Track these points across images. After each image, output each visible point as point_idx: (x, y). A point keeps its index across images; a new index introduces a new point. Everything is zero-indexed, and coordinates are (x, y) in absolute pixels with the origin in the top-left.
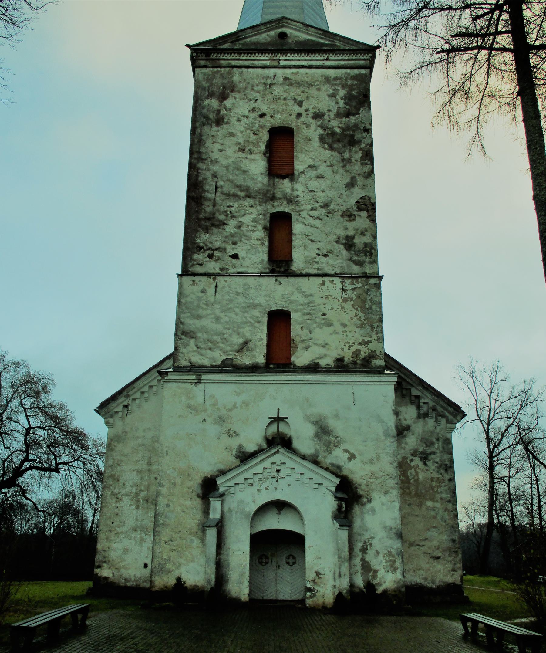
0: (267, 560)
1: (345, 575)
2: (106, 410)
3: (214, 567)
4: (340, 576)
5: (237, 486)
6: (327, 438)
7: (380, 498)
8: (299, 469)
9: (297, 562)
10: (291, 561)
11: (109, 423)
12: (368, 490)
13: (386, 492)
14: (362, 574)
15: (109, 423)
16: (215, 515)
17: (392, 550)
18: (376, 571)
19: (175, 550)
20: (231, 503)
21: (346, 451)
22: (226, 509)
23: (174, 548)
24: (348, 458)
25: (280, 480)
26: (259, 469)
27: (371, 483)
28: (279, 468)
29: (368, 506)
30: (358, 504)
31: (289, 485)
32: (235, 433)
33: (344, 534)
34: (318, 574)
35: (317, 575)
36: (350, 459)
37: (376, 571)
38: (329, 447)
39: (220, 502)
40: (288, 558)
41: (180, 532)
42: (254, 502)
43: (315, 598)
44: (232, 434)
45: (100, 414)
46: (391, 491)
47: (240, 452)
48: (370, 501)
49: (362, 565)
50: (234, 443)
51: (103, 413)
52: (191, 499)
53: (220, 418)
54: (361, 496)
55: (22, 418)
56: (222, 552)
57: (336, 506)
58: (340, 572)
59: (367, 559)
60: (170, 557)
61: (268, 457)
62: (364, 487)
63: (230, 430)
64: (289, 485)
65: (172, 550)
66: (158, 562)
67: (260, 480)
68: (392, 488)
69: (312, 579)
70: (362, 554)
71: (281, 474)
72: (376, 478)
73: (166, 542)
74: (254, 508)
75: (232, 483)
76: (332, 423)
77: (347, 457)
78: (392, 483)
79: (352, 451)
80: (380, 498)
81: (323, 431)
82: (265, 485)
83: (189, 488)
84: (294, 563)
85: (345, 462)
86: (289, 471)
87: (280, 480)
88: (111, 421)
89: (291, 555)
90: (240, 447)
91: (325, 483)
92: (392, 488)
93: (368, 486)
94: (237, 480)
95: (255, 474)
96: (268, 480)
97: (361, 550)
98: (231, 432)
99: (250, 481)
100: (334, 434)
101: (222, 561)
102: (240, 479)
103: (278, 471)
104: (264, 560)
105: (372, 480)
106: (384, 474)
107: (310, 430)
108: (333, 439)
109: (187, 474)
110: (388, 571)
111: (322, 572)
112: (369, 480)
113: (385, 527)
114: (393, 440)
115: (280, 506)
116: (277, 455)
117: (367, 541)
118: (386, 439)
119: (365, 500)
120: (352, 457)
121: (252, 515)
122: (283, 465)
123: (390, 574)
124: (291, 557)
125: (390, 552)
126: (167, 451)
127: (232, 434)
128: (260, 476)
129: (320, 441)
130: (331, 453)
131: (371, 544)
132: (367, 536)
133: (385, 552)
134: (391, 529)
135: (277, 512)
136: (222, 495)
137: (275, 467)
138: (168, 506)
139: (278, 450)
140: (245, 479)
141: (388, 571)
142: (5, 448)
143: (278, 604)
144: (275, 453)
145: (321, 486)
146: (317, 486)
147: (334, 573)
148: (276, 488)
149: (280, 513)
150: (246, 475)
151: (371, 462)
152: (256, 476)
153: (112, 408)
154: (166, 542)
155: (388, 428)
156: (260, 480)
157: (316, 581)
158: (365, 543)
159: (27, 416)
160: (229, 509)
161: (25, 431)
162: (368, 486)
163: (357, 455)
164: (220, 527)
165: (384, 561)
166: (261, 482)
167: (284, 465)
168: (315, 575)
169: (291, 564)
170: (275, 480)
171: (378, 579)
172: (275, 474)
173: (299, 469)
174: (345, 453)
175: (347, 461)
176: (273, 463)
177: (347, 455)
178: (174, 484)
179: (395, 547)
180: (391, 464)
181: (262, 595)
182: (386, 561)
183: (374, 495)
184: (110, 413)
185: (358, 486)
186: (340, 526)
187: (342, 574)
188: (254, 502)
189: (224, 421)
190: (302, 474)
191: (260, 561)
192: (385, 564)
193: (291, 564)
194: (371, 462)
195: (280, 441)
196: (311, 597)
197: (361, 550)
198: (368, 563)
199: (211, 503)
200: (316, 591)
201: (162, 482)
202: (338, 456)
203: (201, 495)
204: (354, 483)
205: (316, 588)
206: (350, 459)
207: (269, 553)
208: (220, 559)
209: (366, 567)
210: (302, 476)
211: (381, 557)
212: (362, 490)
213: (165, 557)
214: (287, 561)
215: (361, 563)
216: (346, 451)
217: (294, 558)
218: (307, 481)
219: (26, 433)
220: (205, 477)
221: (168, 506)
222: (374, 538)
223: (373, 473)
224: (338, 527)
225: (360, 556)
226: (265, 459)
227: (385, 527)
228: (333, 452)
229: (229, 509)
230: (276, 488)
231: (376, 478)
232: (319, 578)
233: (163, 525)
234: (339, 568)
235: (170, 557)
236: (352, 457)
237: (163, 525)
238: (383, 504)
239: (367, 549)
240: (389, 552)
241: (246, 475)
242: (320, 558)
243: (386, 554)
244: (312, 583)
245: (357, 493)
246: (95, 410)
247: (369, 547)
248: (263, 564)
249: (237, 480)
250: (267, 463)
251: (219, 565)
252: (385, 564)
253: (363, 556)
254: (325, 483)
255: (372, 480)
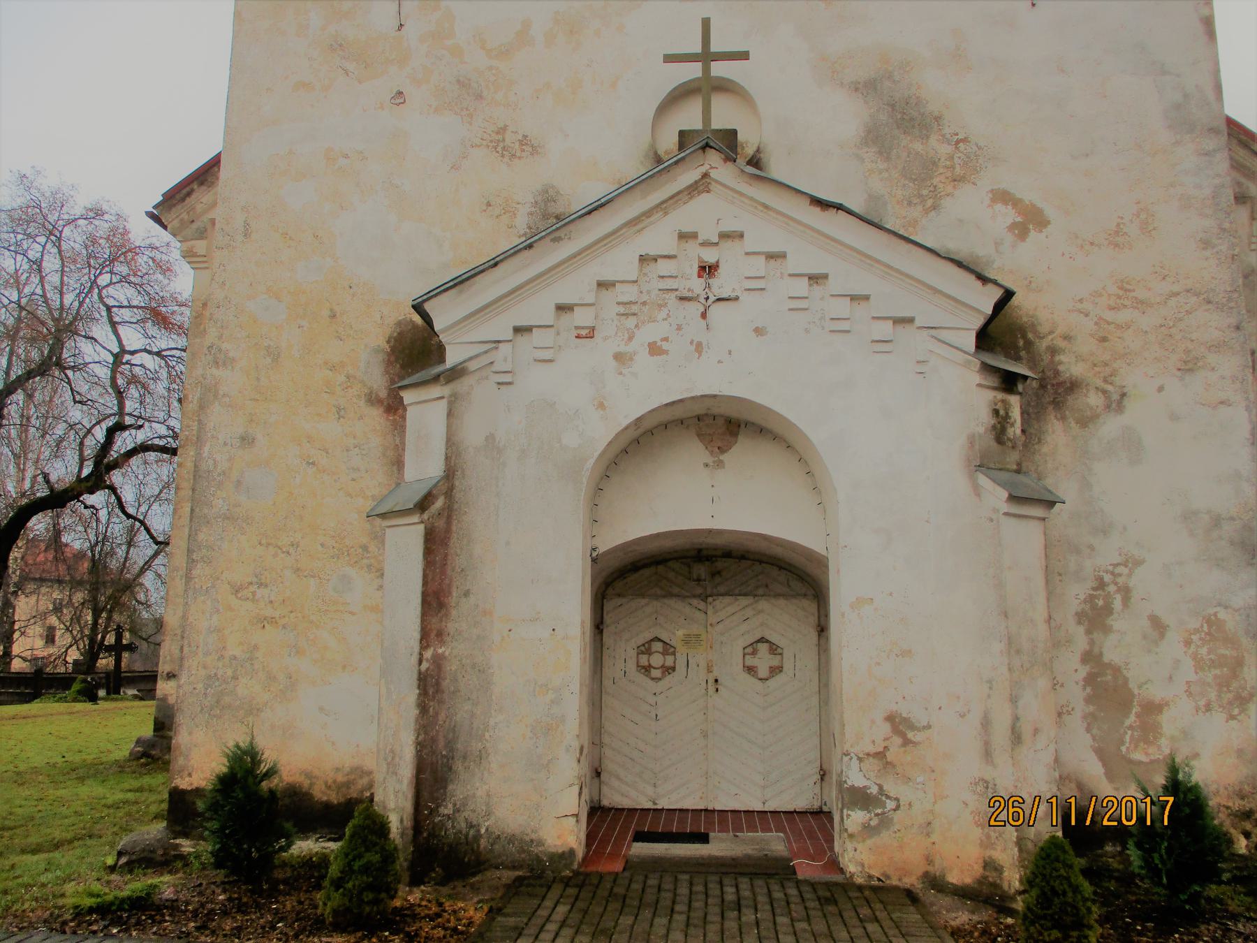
0: (669, 661)
1: (1036, 731)
2: (185, 216)
3: (411, 695)
4: (1016, 738)
5: (522, 340)
6: (918, 146)
7: (1161, 389)
8: (805, 258)
9: (788, 665)
10: (763, 661)
11: (195, 255)
12: (1107, 357)
13: (1188, 367)
14: (1090, 721)
15: (195, 255)
16: (424, 468)
17: (1222, 615)
18: (1153, 708)
19: (272, 621)
20: (489, 412)
21: (1002, 197)
22: (472, 434)
23: (269, 612)
24: (1012, 227)
25: (716, 311)
26: (620, 262)
27: (1119, 327)
28: (710, 256)
29: (1110, 426)
30: (1063, 418)
31: (759, 331)
32: (524, 141)
33: (1025, 539)
34: (899, 724)
35: (896, 730)
36: (1020, 231)
37: (1153, 708)
38: (927, 182)
39: (443, 405)
40: (752, 649)
41: (294, 545)
42: (601, 406)
43: (885, 837)
44: (510, 146)
45: (165, 227)
46: (1212, 358)
47: (545, 216)
48: (1117, 403)
49: (1090, 680)
50: (522, 183)
51: (176, 223)
52: (340, 412)
53: (462, 83)
54: (1073, 386)
55: (101, 331)
56: (451, 627)
57: (982, 419)
58: (1016, 719)
59: (1112, 652)
60: (256, 647)
61: (663, 207)
62: (1086, 345)
63: (502, 130)
64: (759, 331)
65: (264, 622)
66: (203, 672)
67: (628, 310)
68: (1216, 347)
69: (872, 749)
70: (1088, 632)
71: (723, 284)
72: (1142, 305)
73: (237, 590)
74: (599, 433)
75: (499, 327)
76: (935, 86)
77: (1009, 221)
78: (1210, 325)
79: (1029, 195)
80: (1161, 389)
81: (896, 115)
82: (651, 332)
83: (333, 368)
84: (776, 670)
85: (997, 244)
86: (759, 266)
87: (716, 311)
88: (200, 246)
89: (762, 640)
90: (547, 196)
91: (926, 311)
92: (1216, 347)
93: (1104, 339)
94: (523, 313)
95: (602, 285)
96: (663, 314)
97: (1080, 617)
98: (509, 138)
99: (582, 317)
100: (947, 131)
101: (451, 667)
102: (537, 309)
103: (708, 270)
104: (657, 660)
105: (1123, 316)
106: (1176, 288)
107: (843, 118)
108: (945, 150)
109: (326, 313)
110: (1208, 708)
111: (920, 717)
112: (1109, 315)
113: (1189, 516)
114: (1210, 143)
115: (722, 426)
116: (702, 202)
117: (1107, 578)
118: (1177, 143)
119: (1094, 400)
120: (1030, 220)
121: (590, 463)
122: (727, 244)
123: (1219, 717)
124: (763, 648)
125: (1213, 622)
126: (247, 224)
127: (510, 146)
128: (627, 293)
129: (888, 159)
130: (935, 207)
131: (1126, 592)
132: (1107, 554)
133: (1194, 624)
134: (1217, 521)
135: (710, 460)
136: (457, 373)
137: (695, 254)
138: (247, 440)
139: (705, 175)
140: (561, 308)
141: (1208, 708)
142: (75, 402)
143: (720, 846)
144: (694, 189)
145: (904, 332)
146: (886, 329)
147: (986, 723)
148: (699, 347)
149: (720, 464)
150: (565, 291)
151: (1116, 238)
152: (607, 295)
153: (199, 208)
154: (237, 590)
155: (1186, 96)
156: (628, 310)
157: (890, 756)
158: (1101, 585)
159: (114, 325)
160: (490, 438)
161: (111, 359)
162: (1104, 339)
163: (1049, 212)
164: (438, 518)
165: (1188, 663)
166: (631, 322)
167: (737, 243)
168: (886, 728)
169: (763, 672)
170: (695, 309)
171: (1163, 742)
172: (696, 285)
173: (805, 258)
174: (999, 207)
175: (1009, 238)
176: (683, 236)
177: (1008, 215)
178: (275, 355)
179: (1238, 601)
180: (1206, 244)
181: (650, 790)
182: (1199, 665)
183: (1132, 378)
184: (194, 226)
185: (1061, 344)
186: (1014, 499)
187: (1026, 730)
188: (601, 406)
189: (479, 97)
190: (816, 279)
191: (644, 660)
192: (1192, 677)
193: (763, 672)
194: (1116, 238)
195: (708, 142)
196: (868, 830)
197: (1080, 617)
198: (1117, 670)
199: (411, 413)
200: (890, 805)
201: (225, 346)
202: (971, 219)
203: (383, 394)
204: (1043, 329)
205: (891, 788)
206: (1020, 231)
207: (680, 633)
208: (438, 661)
209: (1107, 691)
210: (818, 290)
211: (1172, 646)
212: (1080, 358)
213: (234, 650)
214: (750, 661)
215: (1083, 671)
216: (1002, 197)
217: (774, 649)
218: (842, 308)
219: (114, 363)
220: (399, 323)
221: (247, 440)
222: (1138, 563)
223: (1124, 287)
224: (1005, 507)
225: (1081, 643)
226: (648, 214)
227: (1189, 516)
228: (946, 203)
229: (490, 438)
230: (699, 347)
231: (1141, 305)
232: (907, 742)
233: (228, 517)
234: (1014, 700)
235: (256, 647)
236: (1030, 220)
237: (228, 517)
238: (1174, 417)
239: (1108, 610)
240: (1209, 622)
241: (565, 291)
242: (906, 653)
243: (1196, 631)
244: (872, 765)
245: (1057, 373)
246: (152, 216)
247: (1117, 603)
248: (656, 673)
249: (523, 313)
250: (658, 237)
251: (431, 686)
252: (1192, 677)
253: (1092, 643)
254: (926, 311)
255: (1123, 316)
